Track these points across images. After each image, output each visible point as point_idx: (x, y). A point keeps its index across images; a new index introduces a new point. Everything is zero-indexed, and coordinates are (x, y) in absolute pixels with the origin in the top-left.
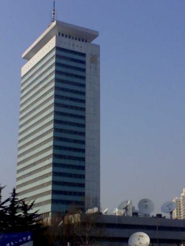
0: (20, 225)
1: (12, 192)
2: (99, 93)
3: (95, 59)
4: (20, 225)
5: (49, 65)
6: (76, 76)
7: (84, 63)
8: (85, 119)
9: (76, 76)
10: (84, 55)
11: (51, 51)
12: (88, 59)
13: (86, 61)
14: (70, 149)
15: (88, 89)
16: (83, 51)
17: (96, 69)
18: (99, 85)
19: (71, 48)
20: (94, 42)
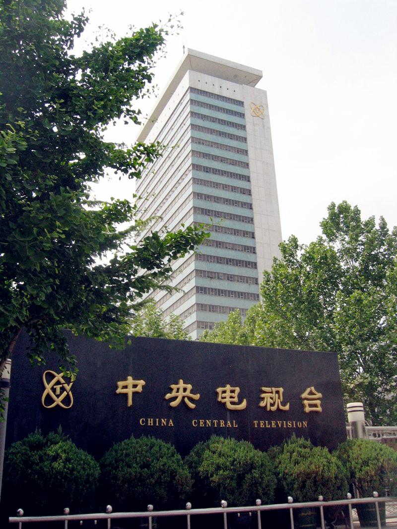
0: (33, 151)
1: (98, 200)
2: (272, 165)
3: (261, 111)
4: (33, 151)
5: (185, 128)
6: (234, 189)
7: (242, 115)
8: (253, 223)
9: (236, 232)
10: (241, 103)
11: (188, 114)
12: (248, 111)
13: (245, 113)
14: (229, 261)
15: (252, 158)
16: (238, 97)
17: (264, 126)
18: (272, 153)
19: (217, 91)
20: (260, 85)
